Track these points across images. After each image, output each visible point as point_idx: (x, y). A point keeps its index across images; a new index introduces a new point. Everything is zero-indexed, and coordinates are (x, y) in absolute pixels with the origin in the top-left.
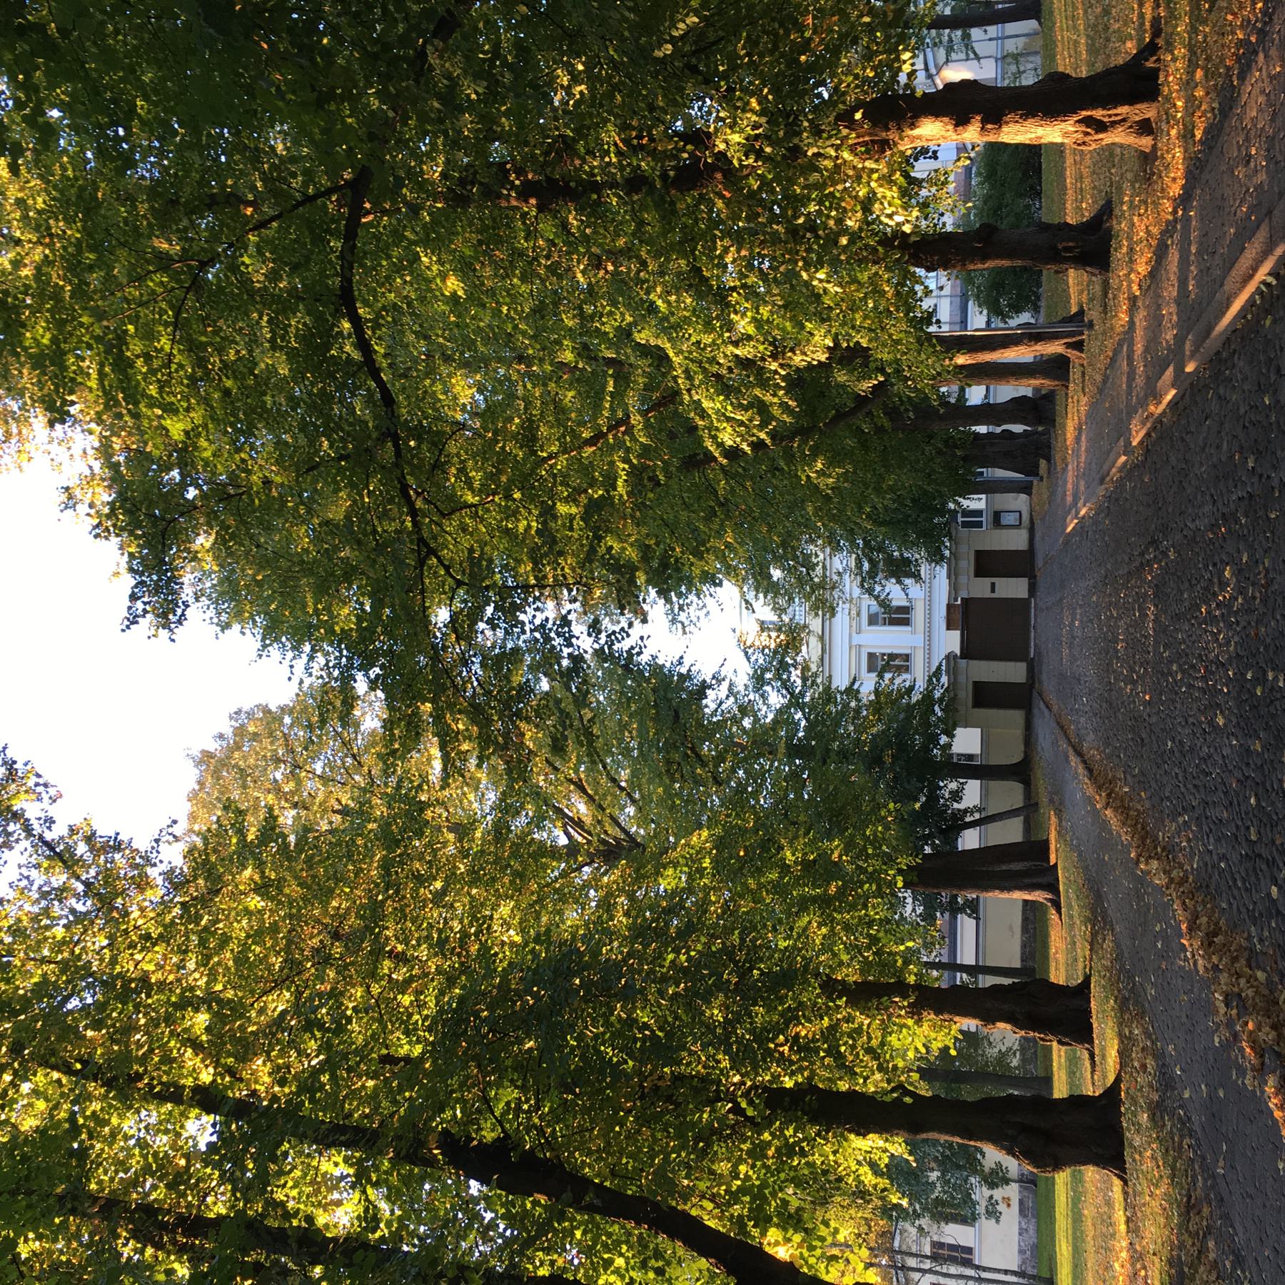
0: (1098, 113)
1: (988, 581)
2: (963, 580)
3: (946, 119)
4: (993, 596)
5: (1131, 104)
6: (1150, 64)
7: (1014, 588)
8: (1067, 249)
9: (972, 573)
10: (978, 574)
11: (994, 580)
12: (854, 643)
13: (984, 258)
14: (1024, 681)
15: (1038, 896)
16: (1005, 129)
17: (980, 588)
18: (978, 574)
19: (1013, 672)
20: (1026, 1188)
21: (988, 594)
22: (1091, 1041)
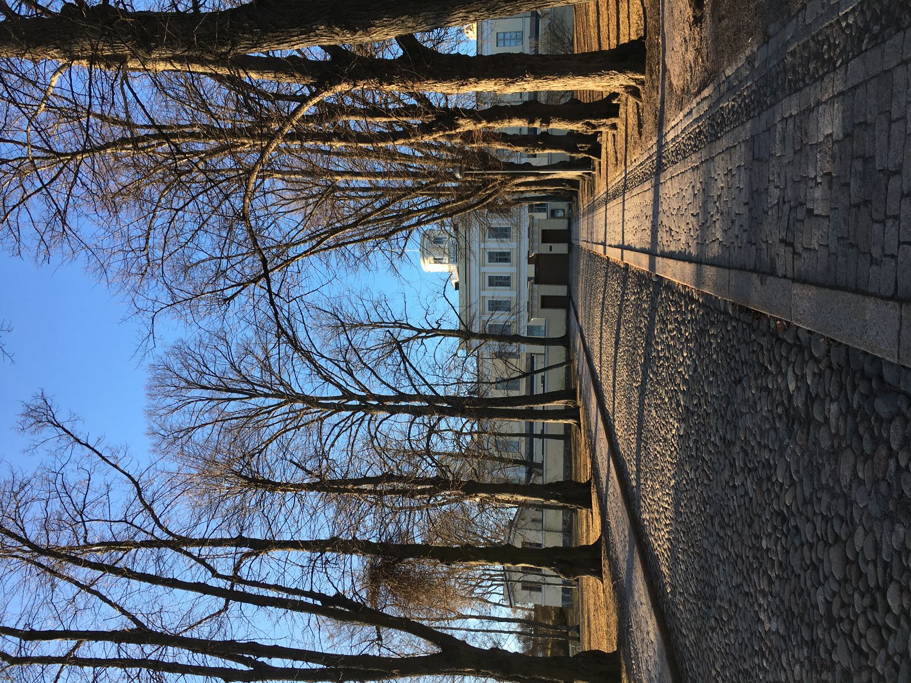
0: (593, 122)
1: (548, 245)
2: (536, 244)
3: (524, 120)
4: (551, 252)
5: (607, 118)
6: (615, 102)
7: (560, 248)
8: (581, 147)
9: (540, 241)
10: (543, 242)
11: (551, 244)
12: (482, 271)
13: (544, 149)
14: (566, 295)
15: (571, 421)
16: (551, 125)
17: (544, 249)
18: (543, 242)
19: (560, 291)
20: (566, 535)
21: (548, 252)
22: (591, 508)
